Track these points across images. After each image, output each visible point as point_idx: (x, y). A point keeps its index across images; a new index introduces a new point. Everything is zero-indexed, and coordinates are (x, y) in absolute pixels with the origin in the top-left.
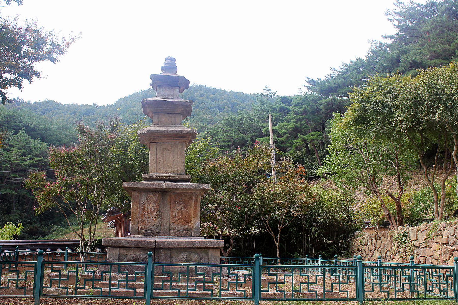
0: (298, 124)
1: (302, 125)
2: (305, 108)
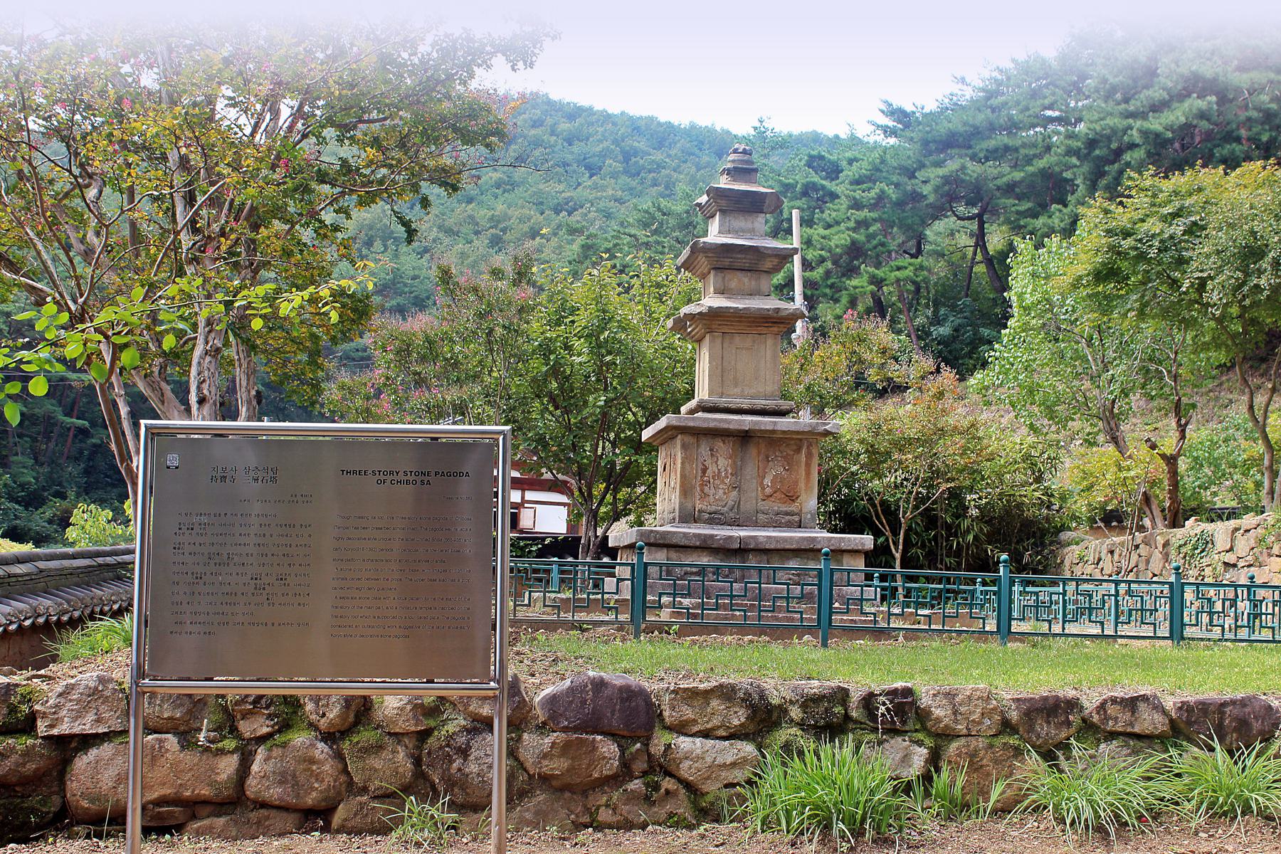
0: (860, 237)
1: (870, 237)
2: (883, 191)
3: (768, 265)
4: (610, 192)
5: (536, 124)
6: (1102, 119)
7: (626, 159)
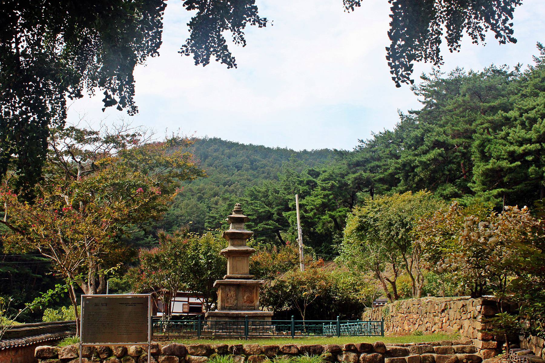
2: (333, 184)
3: (245, 237)
4: (246, 177)
6: (407, 157)
7: (252, 164)
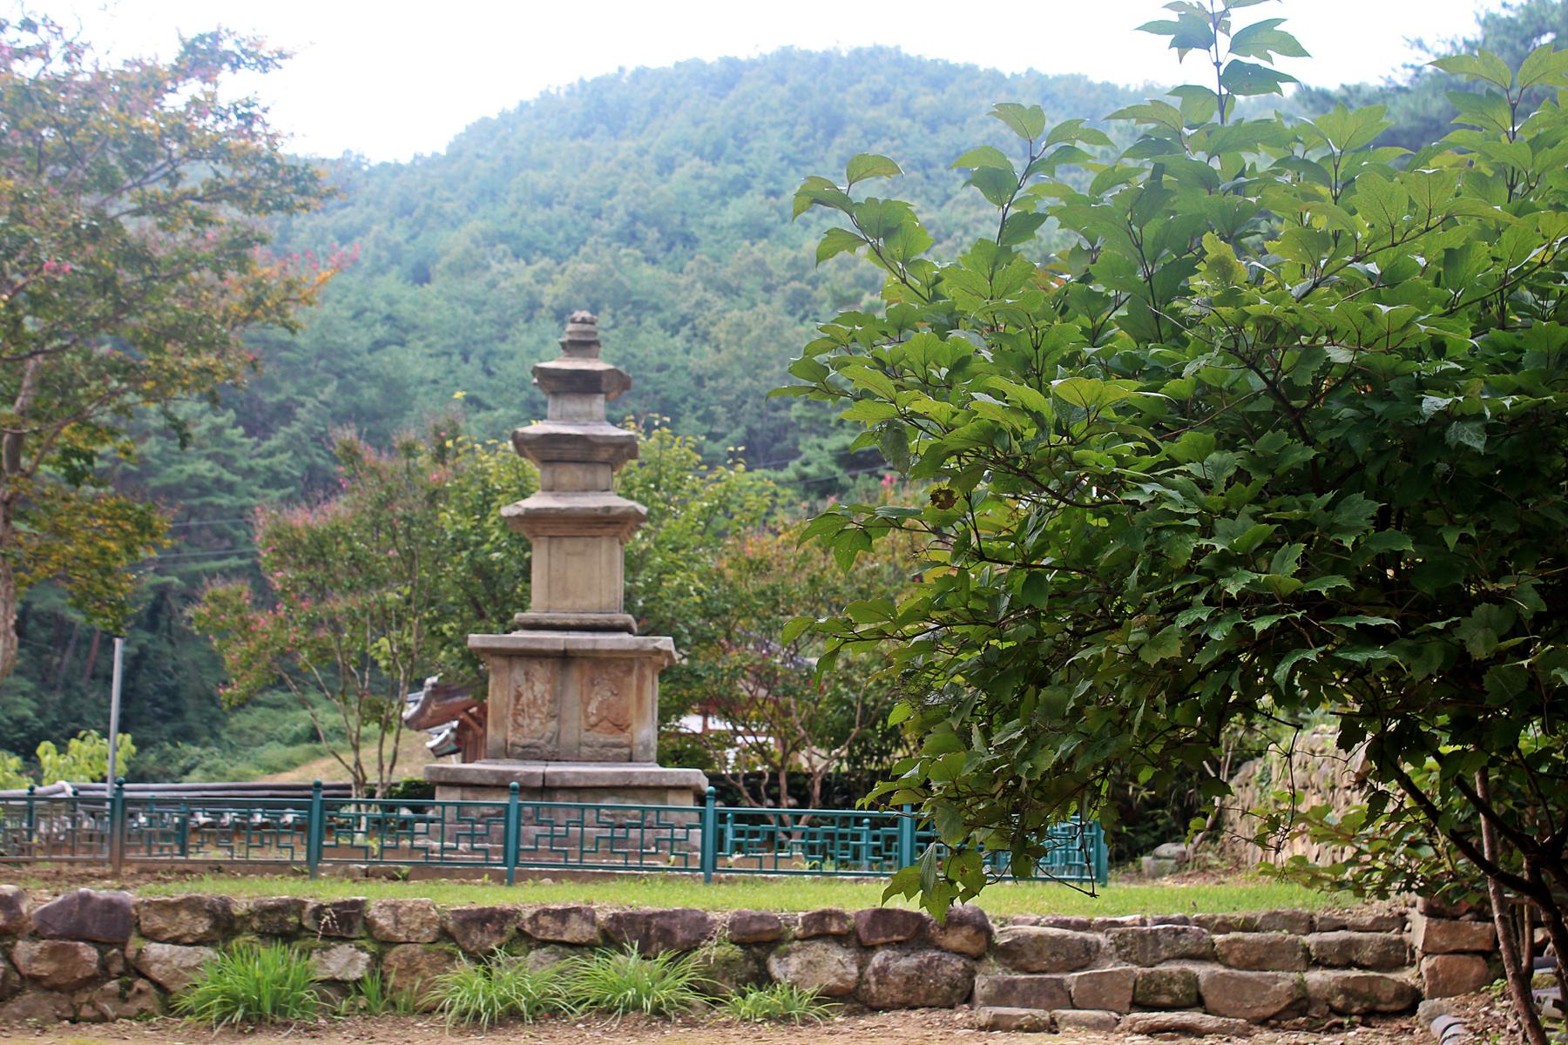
5: (878, 98)
